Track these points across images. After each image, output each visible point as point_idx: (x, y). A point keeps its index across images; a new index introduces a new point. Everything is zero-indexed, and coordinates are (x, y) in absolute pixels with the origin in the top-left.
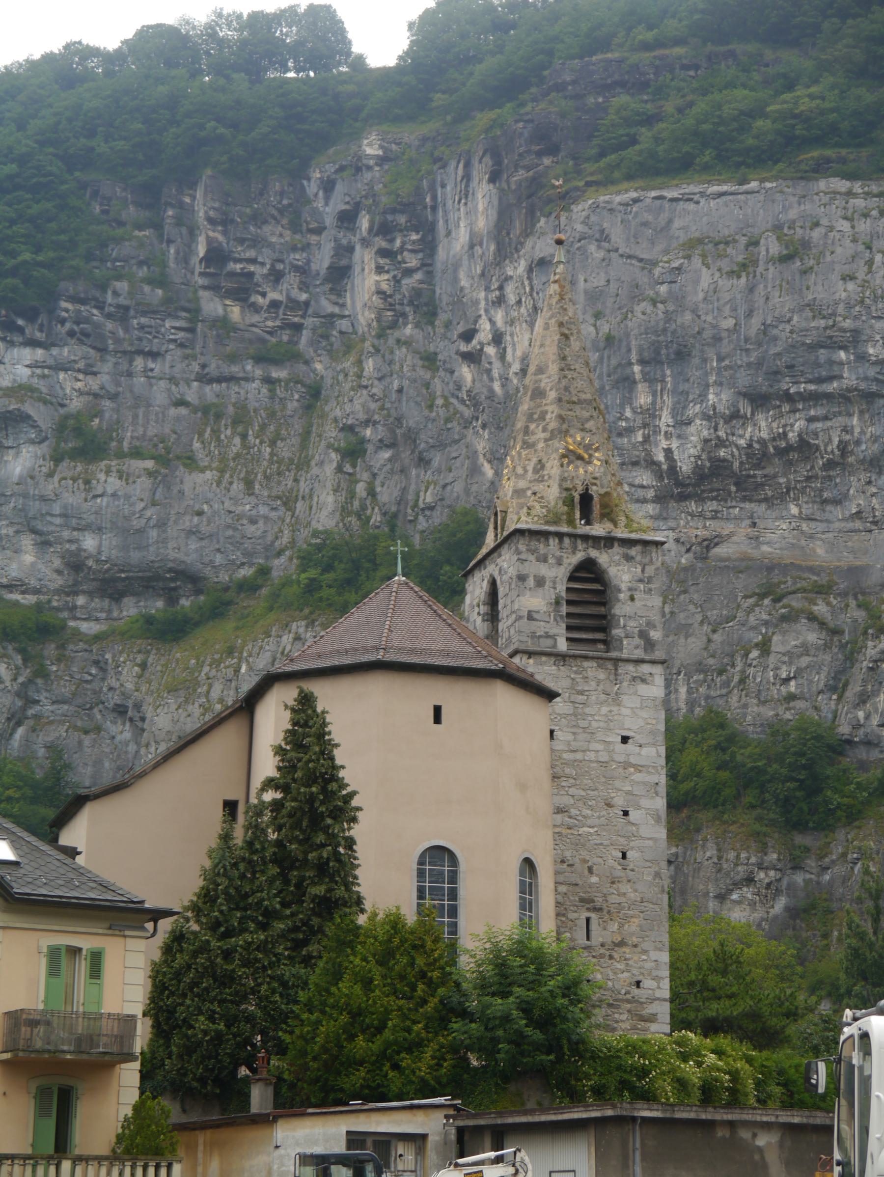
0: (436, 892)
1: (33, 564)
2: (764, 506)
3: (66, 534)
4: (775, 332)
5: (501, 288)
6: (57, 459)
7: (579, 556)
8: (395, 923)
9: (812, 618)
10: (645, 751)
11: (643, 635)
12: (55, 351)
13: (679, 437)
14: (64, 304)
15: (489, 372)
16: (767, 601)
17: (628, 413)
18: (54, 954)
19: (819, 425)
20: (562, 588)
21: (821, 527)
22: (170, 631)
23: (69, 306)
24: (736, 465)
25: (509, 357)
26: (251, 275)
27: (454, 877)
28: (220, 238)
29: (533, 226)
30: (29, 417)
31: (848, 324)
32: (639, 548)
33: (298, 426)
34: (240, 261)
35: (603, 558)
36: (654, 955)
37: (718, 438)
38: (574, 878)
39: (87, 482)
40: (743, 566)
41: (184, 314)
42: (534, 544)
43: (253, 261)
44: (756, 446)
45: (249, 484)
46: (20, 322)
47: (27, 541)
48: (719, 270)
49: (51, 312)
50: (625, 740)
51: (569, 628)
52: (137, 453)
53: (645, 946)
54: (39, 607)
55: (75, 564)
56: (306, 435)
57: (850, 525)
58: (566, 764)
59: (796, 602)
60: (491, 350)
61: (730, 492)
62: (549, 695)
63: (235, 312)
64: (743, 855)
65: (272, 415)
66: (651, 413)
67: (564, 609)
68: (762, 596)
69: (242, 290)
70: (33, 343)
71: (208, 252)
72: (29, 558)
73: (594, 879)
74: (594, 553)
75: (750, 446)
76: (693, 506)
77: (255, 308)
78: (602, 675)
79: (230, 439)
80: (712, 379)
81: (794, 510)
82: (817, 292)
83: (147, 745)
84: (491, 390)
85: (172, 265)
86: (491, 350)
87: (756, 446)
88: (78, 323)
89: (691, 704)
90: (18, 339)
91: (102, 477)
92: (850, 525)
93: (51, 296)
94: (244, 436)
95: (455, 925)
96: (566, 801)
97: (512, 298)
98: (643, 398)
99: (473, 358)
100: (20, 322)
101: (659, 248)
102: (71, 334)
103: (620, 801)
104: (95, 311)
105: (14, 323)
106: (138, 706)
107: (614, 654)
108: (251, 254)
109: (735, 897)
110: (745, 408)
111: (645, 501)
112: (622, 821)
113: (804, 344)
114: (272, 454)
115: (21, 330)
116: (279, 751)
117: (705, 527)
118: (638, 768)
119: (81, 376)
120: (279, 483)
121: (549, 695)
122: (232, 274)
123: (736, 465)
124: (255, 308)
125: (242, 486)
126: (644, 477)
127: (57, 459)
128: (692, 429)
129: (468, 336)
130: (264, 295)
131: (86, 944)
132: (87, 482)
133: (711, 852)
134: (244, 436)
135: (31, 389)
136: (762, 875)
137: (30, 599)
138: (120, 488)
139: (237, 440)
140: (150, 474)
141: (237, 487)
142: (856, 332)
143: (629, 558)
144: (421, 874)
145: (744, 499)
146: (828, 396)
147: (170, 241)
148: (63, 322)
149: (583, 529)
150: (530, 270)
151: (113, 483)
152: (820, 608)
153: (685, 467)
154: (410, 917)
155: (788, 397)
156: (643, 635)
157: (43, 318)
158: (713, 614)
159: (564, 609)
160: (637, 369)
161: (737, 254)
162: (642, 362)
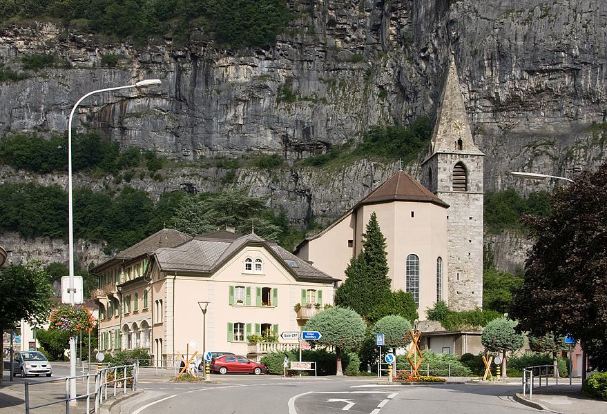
0: (411, 273)
1: (271, 141)
2: (531, 112)
3: (282, 130)
4: (538, 46)
5: (436, 31)
6: (278, 101)
7: (457, 161)
8: (401, 293)
9: (548, 154)
10: (477, 222)
11: (477, 185)
12: (276, 61)
13: (501, 88)
14: (279, 44)
15: (432, 64)
16: (531, 148)
17: (483, 79)
18: (304, 291)
19: (553, 81)
20: (452, 171)
21: (552, 120)
22: (318, 163)
23: (281, 44)
24: (522, 97)
25: (439, 58)
26: (345, 29)
27: (417, 263)
28: (334, 15)
29: (449, 7)
30: (268, 87)
31: (565, 42)
32: (476, 157)
33: (363, 86)
34: (341, 24)
35: (464, 161)
36: (478, 284)
37: (515, 87)
38: (454, 262)
39: (289, 110)
40: (525, 135)
41: (321, 45)
42: (443, 157)
43: (345, 24)
44: (529, 90)
45: (346, 109)
46: (264, 51)
47: (269, 132)
48: (518, 22)
49: (274, 47)
50: (471, 218)
51: (454, 183)
52: (306, 99)
53: (475, 281)
54: (274, 156)
55: (285, 140)
56: (366, 89)
57: (563, 119)
58: (452, 226)
59: (542, 148)
60: (433, 56)
61: (518, 108)
62: (446, 206)
63: (339, 43)
64: (519, 239)
65: (353, 82)
66: (491, 78)
67: (452, 177)
68: (529, 146)
69: (342, 35)
70: (267, 59)
71: (329, 21)
72: (270, 138)
73: (460, 262)
74: (462, 159)
75: (527, 90)
76: (505, 113)
77: (346, 41)
78: (463, 198)
79: (338, 92)
80: (514, 65)
81: (543, 114)
82: (556, 30)
83: (313, 204)
84: (433, 71)
85: (317, 26)
86: (433, 56)
87: (529, 90)
88: (284, 51)
89: (503, 186)
90: (263, 57)
91: (294, 107)
92: (563, 119)
93: (274, 41)
94: (344, 90)
95: (418, 277)
96: (451, 238)
97: (441, 35)
98: (488, 73)
99: (426, 59)
100: (264, 51)
101: (496, 14)
102: (281, 55)
103: (469, 238)
104: (290, 46)
105: (261, 51)
106: (309, 191)
107: (468, 192)
108: (345, 21)
109: (515, 254)
110: (526, 75)
111: (488, 112)
112: (469, 243)
113: (548, 50)
114: (353, 97)
115: (264, 54)
116: (368, 227)
117: (509, 121)
118: (474, 227)
119: (285, 71)
120: (356, 108)
121: (446, 206)
122: (338, 30)
123: (522, 97)
124: (346, 41)
125: (343, 110)
126: (488, 103)
127: (278, 101)
128: (506, 84)
129: (424, 50)
130: (350, 36)
131: (318, 289)
132: (289, 110)
133: (508, 239)
134: (344, 90)
135: (268, 76)
136: (525, 246)
137: (271, 153)
138: (304, 112)
139: (341, 92)
140: (310, 106)
141: (342, 110)
142: (569, 45)
143: (473, 161)
144: (408, 262)
145: (524, 110)
146: (557, 70)
147: (315, 17)
148: (278, 50)
149: (460, 152)
150: (447, 24)
151: (299, 110)
152: (550, 150)
153: (503, 99)
154: (404, 290)
155: (542, 71)
156: (477, 185)
157: (271, 49)
158: (511, 154)
159: (452, 177)
160: (486, 62)
161: (524, 15)
162: (488, 59)
